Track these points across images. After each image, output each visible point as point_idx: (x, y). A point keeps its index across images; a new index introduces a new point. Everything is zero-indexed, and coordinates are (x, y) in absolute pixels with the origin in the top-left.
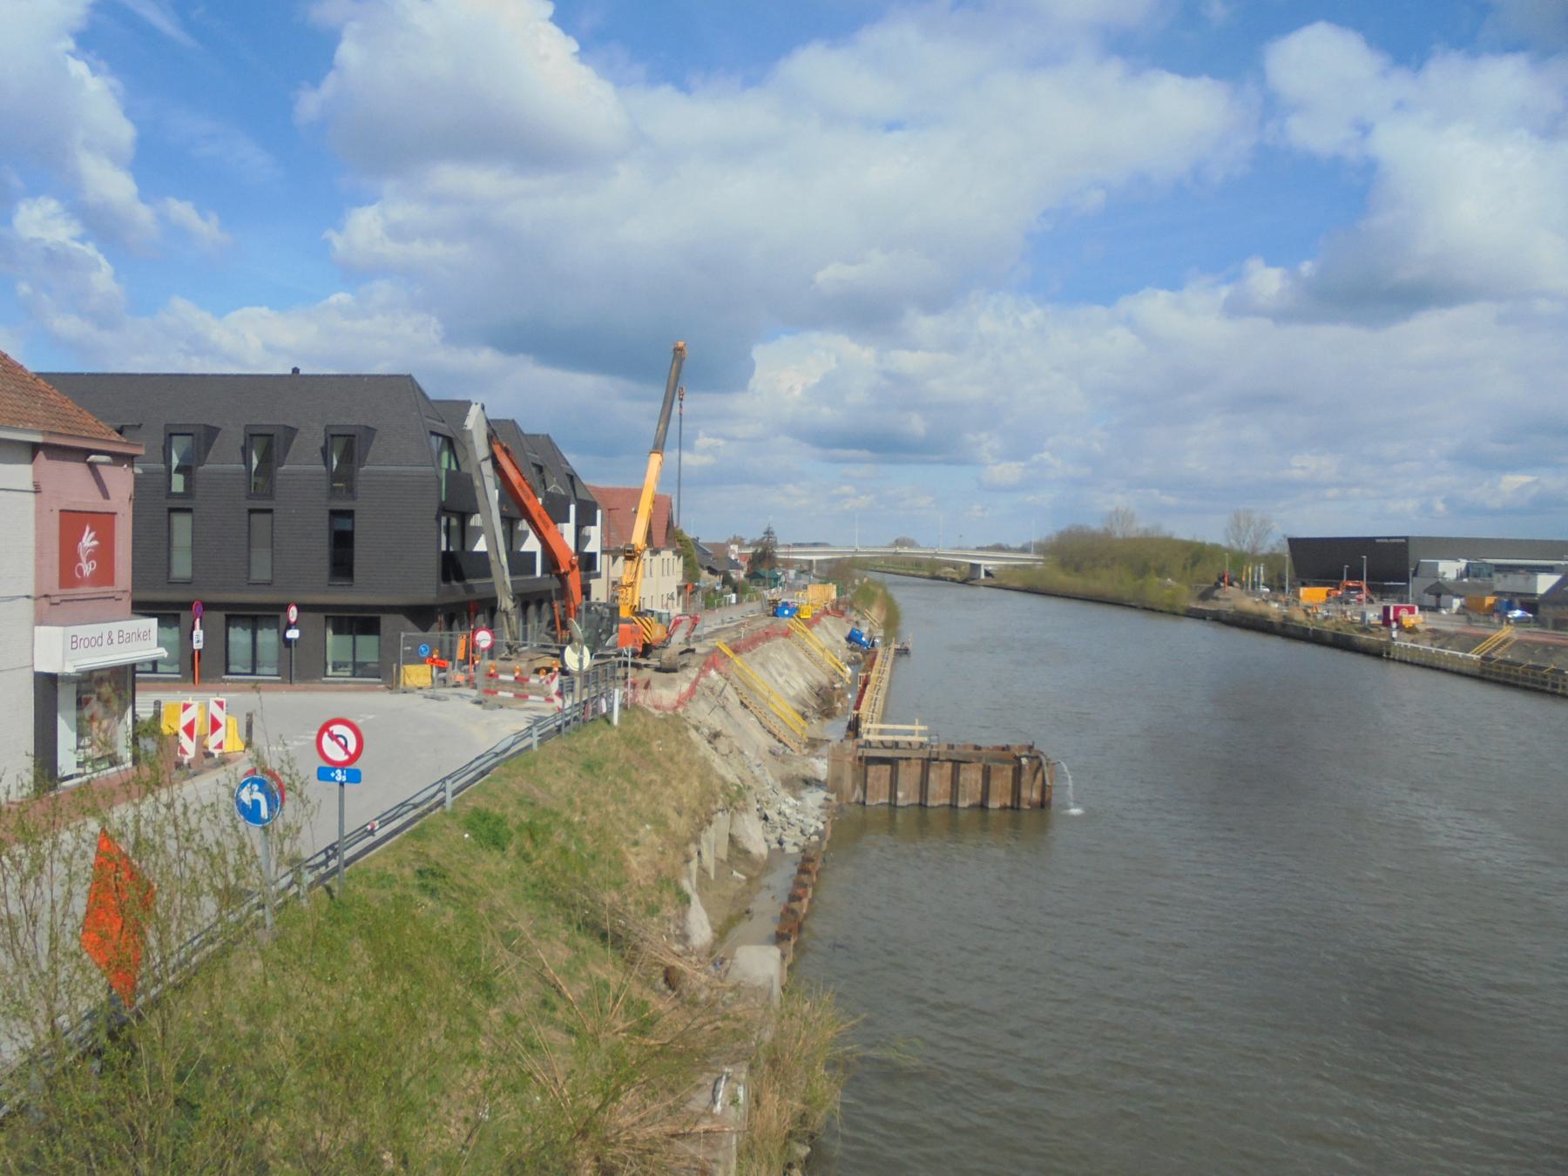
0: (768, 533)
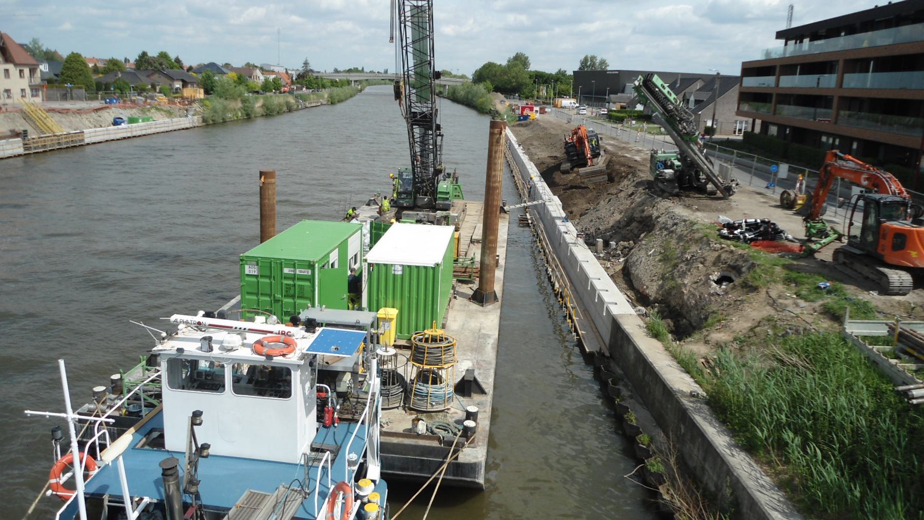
0: (306, 64)
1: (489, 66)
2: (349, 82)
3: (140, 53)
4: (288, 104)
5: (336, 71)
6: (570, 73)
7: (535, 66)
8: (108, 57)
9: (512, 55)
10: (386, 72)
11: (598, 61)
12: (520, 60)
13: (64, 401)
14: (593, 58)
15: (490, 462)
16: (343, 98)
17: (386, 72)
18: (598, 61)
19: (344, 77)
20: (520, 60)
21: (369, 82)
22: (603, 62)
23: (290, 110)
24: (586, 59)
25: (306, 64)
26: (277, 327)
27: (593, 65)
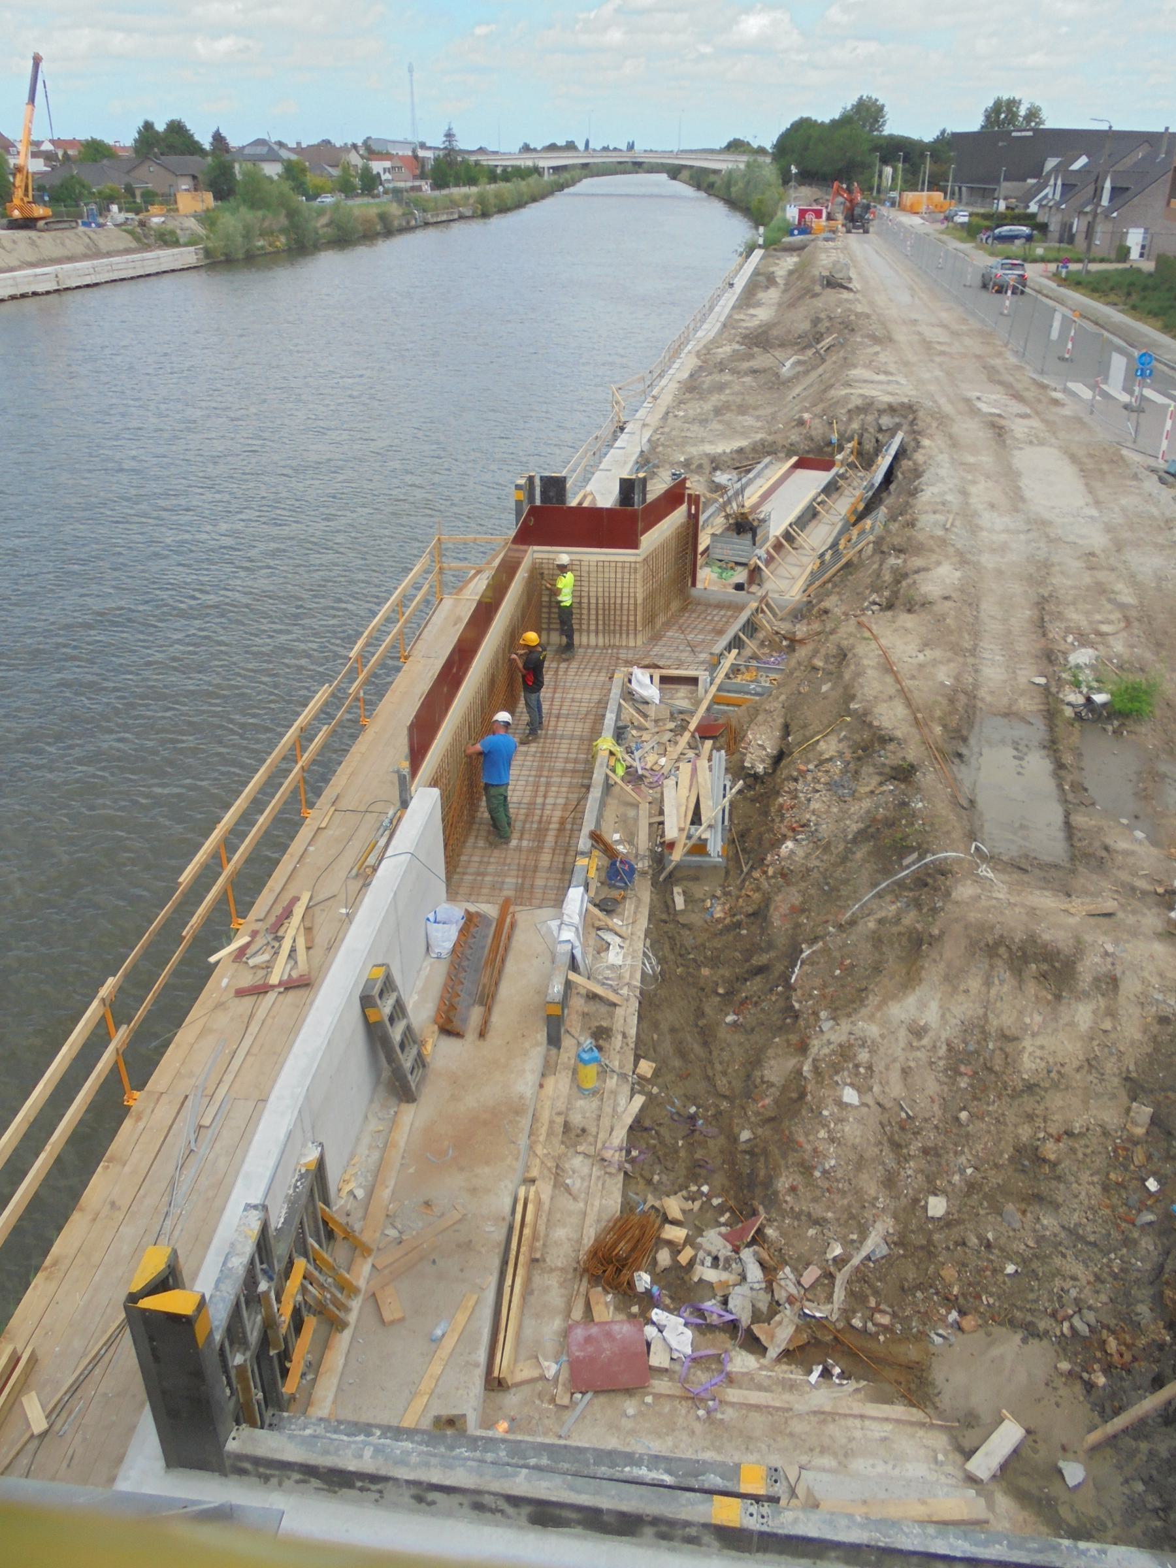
0: (449, 135)
1: (802, 127)
2: (536, 170)
3: (141, 124)
4: (383, 217)
5: (526, 148)
6: (768, 146)
7: (895, 126)
8: (83, 135)
9: (850, 102)
10: (631, 147)
11: (1023, 112)
12: (867, 113)
13: (25, 1174)
14: (1012, 104)
15: (643, 1036)
16: (509, 203)
17: (631, 147)
18: (1023, 112)
19: (527, 162)
20: (867, 113)
21: (588, 170)
23: (389, 233)
24: (998, 107)
25: (449, 135)
26: (1026, 1055)
27: (1012, 115)
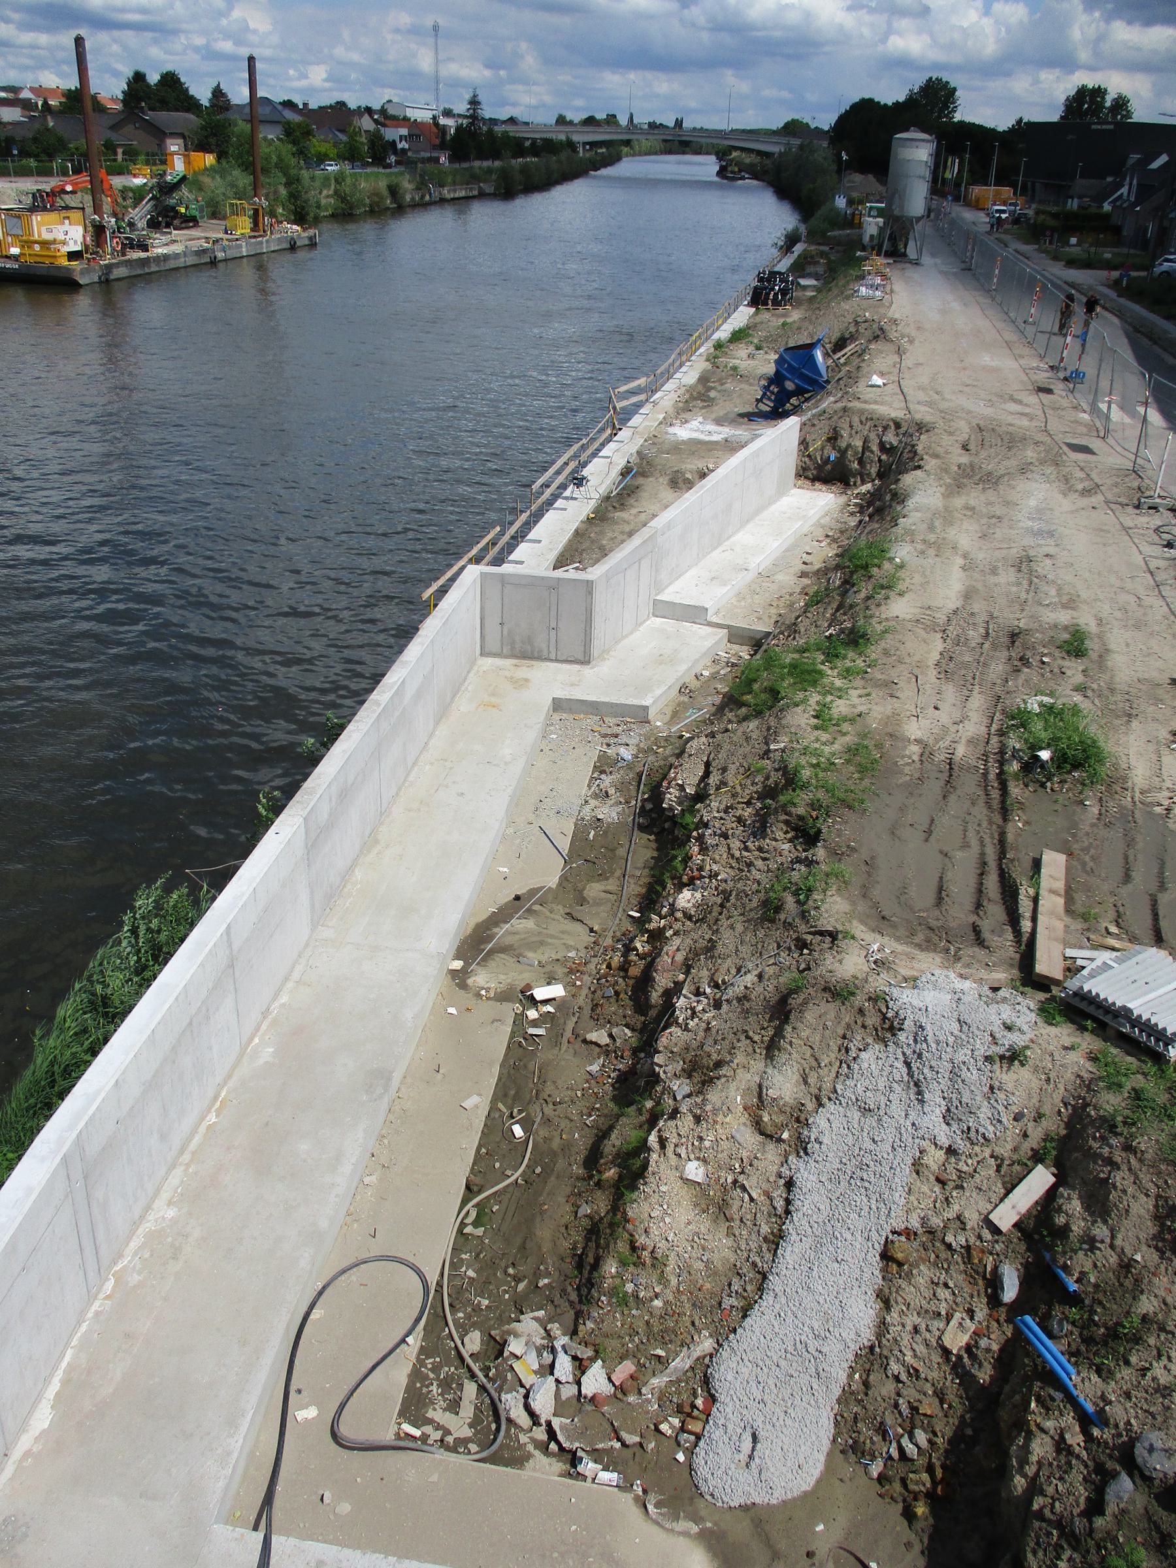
0: (474, 102)
5: (561, 120)
22: (1121, 104)
